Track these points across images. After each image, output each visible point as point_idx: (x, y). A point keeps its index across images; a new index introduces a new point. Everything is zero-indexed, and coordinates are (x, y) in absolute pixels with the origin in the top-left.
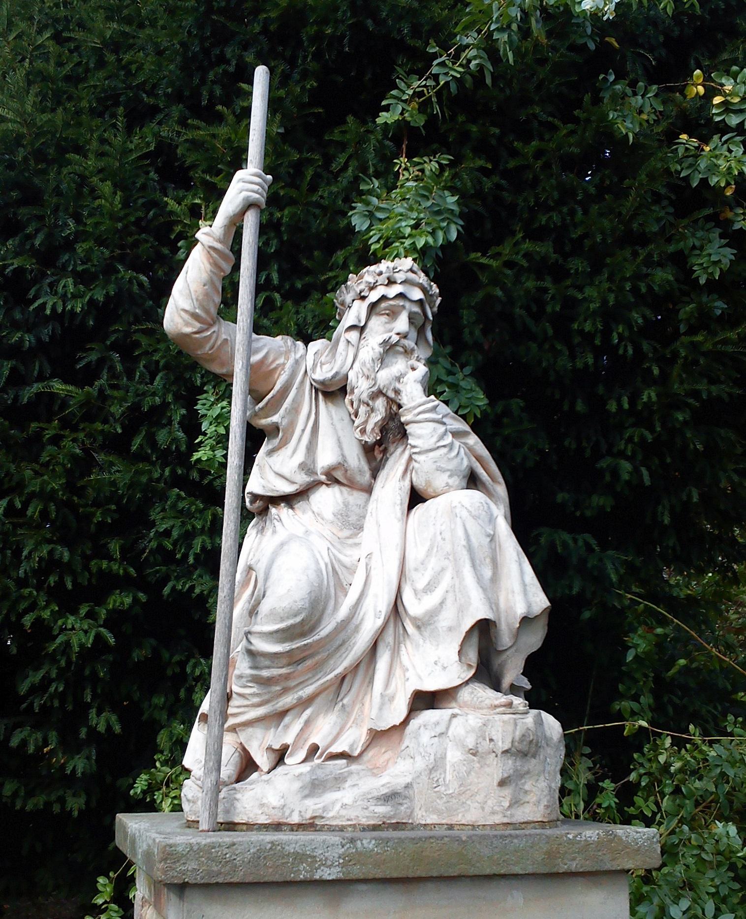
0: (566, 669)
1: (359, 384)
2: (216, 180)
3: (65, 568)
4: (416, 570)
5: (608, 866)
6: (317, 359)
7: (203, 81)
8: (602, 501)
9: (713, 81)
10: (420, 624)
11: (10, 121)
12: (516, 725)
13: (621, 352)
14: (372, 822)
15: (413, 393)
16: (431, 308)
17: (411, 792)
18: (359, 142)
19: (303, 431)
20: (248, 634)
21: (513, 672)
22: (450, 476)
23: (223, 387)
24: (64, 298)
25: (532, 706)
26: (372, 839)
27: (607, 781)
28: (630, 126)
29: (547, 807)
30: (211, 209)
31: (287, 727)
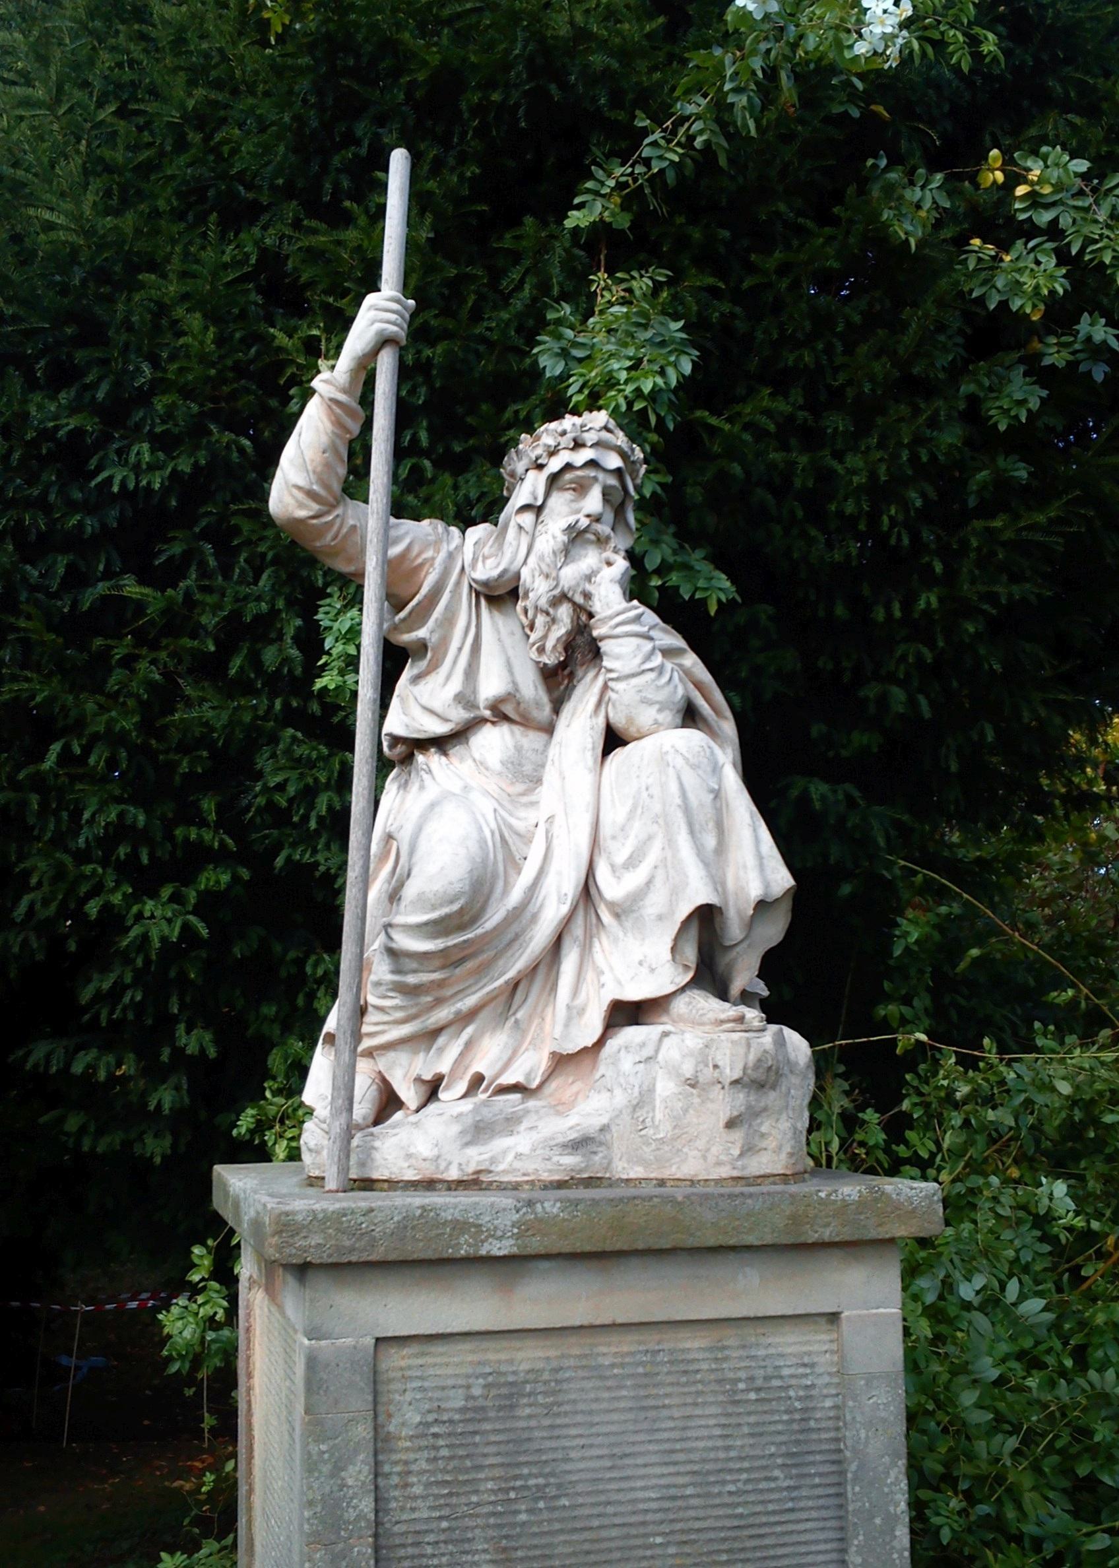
0: (817, 969)
1: (536, 585)
2: (343, 303)
3: (139, 837)
4: (614, 838)
5: (873, 1234)
6: (478, 552)
7: (324, 168)
8: (865, 740)
9: (1017, 165)
10: (620, 911)
11: (62, 227)
12: (749, 1046)
13: (893, 541)
14: (556, 1177)
15: (609, 598)
16: (633, 480)
17: (608, 1137)
18: (539, 252)
19: (460, 649)
20: (387, 927)
21: (745, 974)
22: (660, 710)
23: (352, 590)
24: (137, 468)
25: (770, 1021)
26: (556, 1201)
27: (869, 1111)
28: (910, 228)
29: (791, 1155)
30: (334, 343)
31: (441, 1050)
